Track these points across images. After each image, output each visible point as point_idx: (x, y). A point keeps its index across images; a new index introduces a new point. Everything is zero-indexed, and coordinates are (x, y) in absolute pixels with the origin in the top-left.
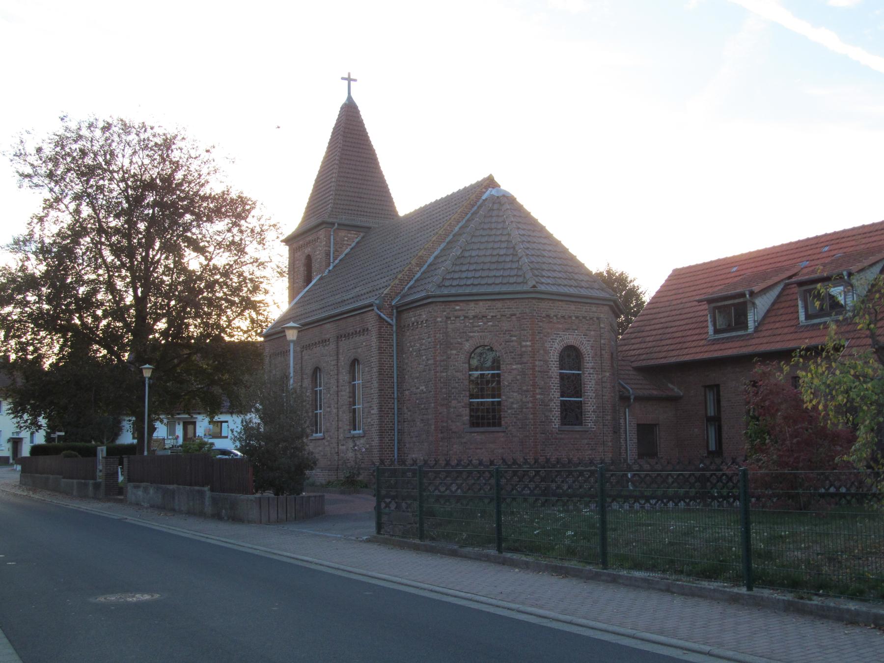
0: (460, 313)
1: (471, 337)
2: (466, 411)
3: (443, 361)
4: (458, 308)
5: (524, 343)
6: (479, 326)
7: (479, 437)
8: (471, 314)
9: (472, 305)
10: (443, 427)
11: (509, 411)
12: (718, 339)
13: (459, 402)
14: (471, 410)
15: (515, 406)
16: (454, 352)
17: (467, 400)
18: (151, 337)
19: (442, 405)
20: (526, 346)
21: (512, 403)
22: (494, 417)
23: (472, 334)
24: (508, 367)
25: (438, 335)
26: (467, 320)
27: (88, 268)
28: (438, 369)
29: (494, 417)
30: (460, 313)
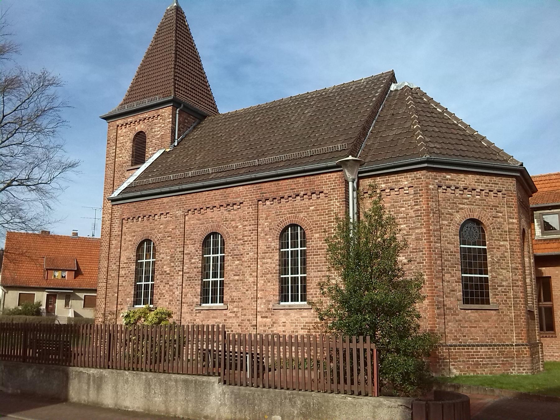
0: (452, 183)
1: (462, 209)
2: (460, 287)
3: (437, 231)
4: (448, 177)
5: (511, 220)
6: (468, 198)
7: (473, 315)
8: (462, 185)
9: (462, 176)
10: (439, 302)
11: (500, 289)
12: (545, 240)
13: (453, 276)
14: (465, 286)
15: (504, 283)
16: (445, 222)
17: (459, 274)
18: (20, 308)
19: (437, 278)
20: (513, 223)
21: (502, 280)
22: (482, 293)
23: (461, 206)
24: (496, 243)
25: (430, 203)
26: (457, 190)
27: (15, 140)
28: (432, 239)
29: (482, 293)
30: (452, 183)
